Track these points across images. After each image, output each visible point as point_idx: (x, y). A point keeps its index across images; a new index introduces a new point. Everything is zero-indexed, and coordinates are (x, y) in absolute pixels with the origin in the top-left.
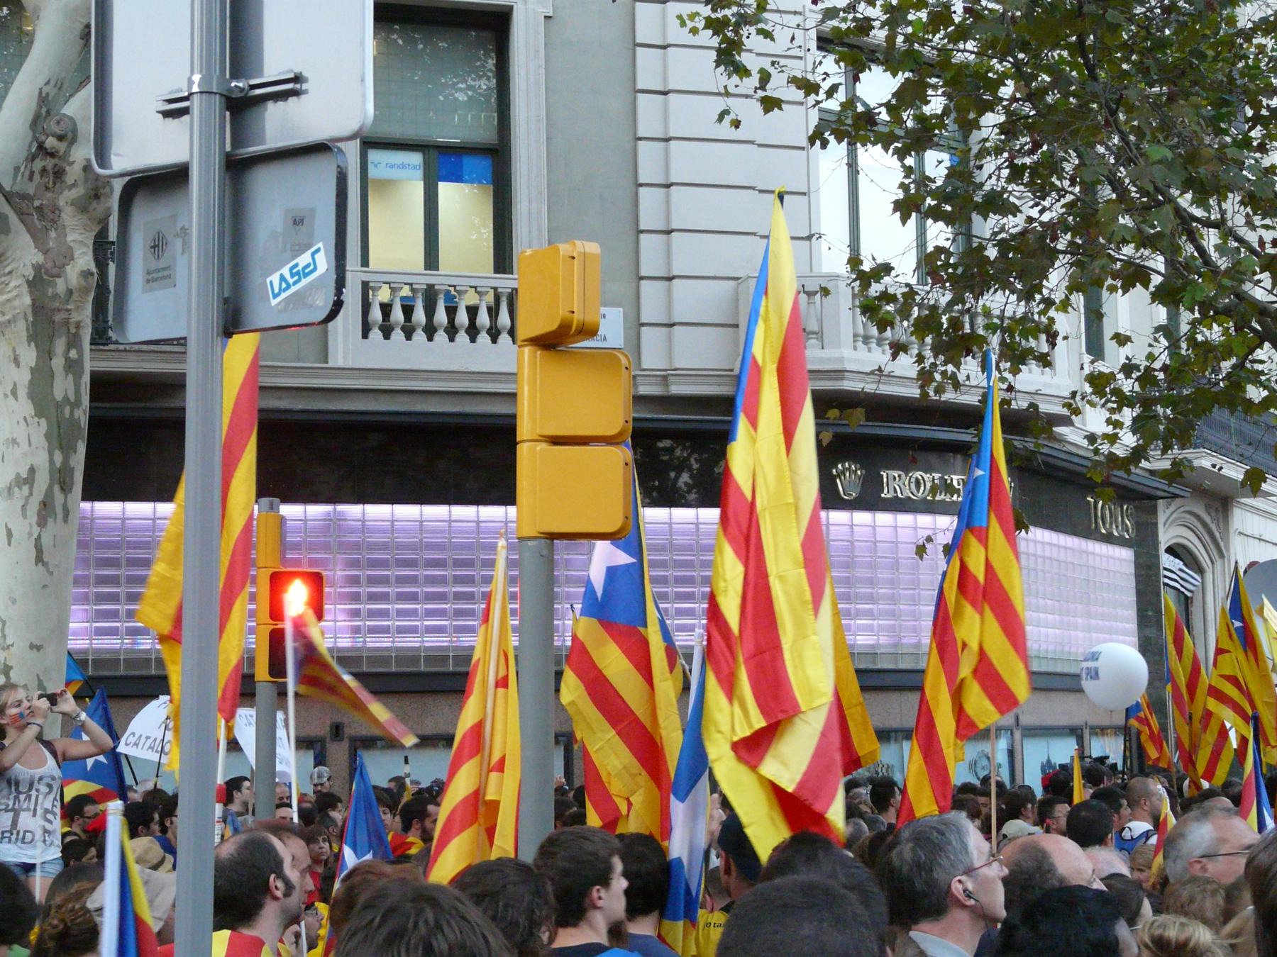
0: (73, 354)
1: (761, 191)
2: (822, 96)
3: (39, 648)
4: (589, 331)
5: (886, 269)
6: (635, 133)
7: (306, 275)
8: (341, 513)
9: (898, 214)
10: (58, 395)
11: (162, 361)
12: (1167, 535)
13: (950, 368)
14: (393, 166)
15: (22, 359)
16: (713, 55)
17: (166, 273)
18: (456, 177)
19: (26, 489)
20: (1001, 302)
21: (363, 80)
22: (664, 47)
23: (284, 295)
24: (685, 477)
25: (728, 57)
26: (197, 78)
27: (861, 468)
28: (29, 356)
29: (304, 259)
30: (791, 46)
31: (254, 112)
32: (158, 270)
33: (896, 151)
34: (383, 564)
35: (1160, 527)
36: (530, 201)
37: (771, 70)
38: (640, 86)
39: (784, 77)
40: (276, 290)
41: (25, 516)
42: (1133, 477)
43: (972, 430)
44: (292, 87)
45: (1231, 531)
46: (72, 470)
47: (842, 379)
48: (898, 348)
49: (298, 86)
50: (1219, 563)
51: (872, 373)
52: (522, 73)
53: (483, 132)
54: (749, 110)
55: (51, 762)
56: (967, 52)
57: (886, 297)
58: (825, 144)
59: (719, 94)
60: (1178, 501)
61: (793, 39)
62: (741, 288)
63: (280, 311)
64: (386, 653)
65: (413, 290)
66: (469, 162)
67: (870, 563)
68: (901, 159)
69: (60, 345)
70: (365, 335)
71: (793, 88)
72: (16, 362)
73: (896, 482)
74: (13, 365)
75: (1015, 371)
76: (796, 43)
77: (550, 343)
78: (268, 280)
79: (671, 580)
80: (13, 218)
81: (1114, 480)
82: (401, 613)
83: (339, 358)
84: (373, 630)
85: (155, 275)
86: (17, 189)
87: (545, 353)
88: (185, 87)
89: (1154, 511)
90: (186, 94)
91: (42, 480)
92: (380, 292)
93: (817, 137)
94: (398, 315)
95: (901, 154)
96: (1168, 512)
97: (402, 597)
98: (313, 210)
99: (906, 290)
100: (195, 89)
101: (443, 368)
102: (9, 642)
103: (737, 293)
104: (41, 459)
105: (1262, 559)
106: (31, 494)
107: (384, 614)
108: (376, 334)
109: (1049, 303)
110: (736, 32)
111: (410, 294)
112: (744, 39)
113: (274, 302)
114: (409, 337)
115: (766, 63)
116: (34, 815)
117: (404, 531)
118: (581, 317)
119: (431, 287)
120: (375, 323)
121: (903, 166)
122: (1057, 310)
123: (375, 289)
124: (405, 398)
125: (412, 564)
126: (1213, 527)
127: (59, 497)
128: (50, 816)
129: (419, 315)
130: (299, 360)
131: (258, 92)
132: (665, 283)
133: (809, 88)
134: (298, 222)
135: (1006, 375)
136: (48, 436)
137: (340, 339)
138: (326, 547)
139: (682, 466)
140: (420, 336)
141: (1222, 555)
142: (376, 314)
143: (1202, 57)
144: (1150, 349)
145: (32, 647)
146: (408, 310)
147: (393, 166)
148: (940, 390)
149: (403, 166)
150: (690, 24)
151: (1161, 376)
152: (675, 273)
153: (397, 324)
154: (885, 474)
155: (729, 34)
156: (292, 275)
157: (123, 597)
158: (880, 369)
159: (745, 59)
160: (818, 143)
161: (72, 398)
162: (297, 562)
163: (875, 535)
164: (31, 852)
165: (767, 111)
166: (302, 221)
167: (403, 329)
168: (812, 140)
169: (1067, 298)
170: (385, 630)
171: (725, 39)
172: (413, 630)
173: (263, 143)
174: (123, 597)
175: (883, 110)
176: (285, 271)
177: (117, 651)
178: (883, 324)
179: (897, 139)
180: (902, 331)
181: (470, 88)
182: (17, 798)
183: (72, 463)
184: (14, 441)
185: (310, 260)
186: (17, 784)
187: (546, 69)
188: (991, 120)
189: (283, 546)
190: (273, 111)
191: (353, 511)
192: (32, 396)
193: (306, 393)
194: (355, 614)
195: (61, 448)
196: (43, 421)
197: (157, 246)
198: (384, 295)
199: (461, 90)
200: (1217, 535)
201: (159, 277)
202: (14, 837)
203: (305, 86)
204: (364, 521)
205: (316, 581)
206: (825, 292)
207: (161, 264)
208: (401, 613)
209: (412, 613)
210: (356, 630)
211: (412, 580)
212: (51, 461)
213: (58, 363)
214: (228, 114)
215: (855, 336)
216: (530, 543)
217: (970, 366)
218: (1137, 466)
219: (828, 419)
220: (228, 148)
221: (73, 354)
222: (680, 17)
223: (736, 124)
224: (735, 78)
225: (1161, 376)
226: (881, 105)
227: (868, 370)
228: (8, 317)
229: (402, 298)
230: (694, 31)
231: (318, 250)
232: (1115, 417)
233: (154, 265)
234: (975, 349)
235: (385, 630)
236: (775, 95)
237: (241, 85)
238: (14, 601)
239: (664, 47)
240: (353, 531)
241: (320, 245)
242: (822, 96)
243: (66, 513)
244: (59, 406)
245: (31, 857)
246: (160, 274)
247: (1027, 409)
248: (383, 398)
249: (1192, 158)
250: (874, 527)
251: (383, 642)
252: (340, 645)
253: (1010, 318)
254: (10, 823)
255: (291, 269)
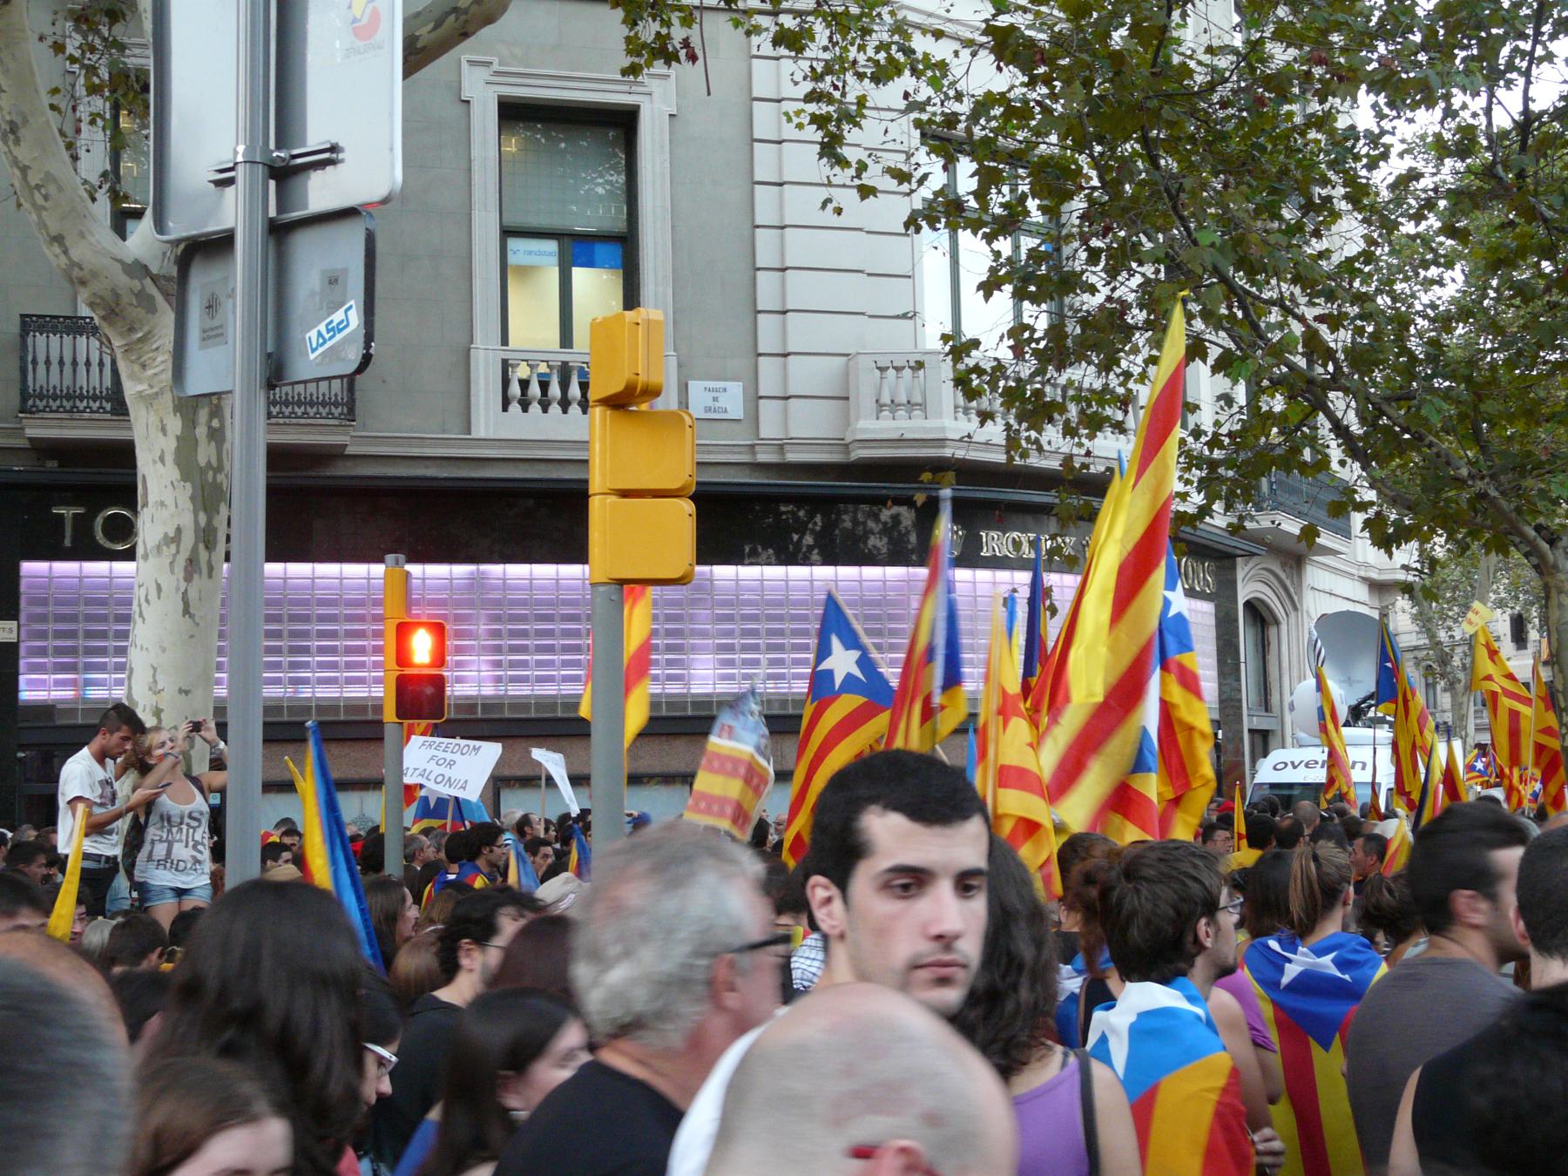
0: (215, 423)
1: (869, 275)
2: (914, 186)
3: (187, 692)
4: (652, 392)
5: (976, 344)
6: (753, 220)
7: (340, 331)
8: (483, 573)
9: (981, 292)
10: (202, 461)
11: (321, 434)
12: (1244, 592)
13: (1033, 434)
14: (530, 253)
15: (168, 428)
16: (817, 148)
17: (219, 331)
18: (590, 263)
19: (173, 547)
20: (1084, 375)
21: (391, 149)
22: (780, 142)
23: (320, 350)
24: (809, 540)
25: (830, 149)
26: (241, 148)
27: (962, 529)
28: (175, 425)
29: (338, 316)
30: (885, 139)
31: (297, 181)
32: (212, 329)
33: (985, 236)
34: (523, 619)
35: (1240, 585)
36: (656, 285)
37: (869, 162)
38: (757, 178)
39: (879, 168)
40: (314, 346)
41: (172, 572)
42: (1198, 533)
43: (1053, 492)
44: (330, 157)
45: (1305, 585)
46: (215, 530)
47: (943, 447)
48: (985, 416)
49: (334, 156)
50: (1293, 615)
51: (961, 440)
52: (649, 166)
53: (620, 225)
54: (848, 198)
55: (199, 797)
56: (1050, 145)
57: (977, 370)
58: (918, 230)
59: (823, 185)
60: (1255, 560)
61: (886, 132)
62: (851, 363)
63: (318, 365)
64: (524, 701)
65: (549, 366)
66: (601, 250)
67: (971, 616)
68: (989, 243)
69: (203, 415)
70: (505, 409)
71: (887, 177)
72: (164, 430)
73: (995, 542)
74: (161, 434)
75: (1091, 437)
76: (890, 136)
77: (619, 403)
78: (307, 336)
79: (788, 632)
80: (159, 298)
81: (1182, 535)
82: (540, 664)
83: (480, 430)
84: (514, 679)
85: (210, 333)
86: (163, 272)
87: (617, 414)
88: (231, 156)
89: (1233, 568)
90: (231, 165)
91: (188, 539)
92: (518, 369)
93: (912, 223)
94: (535, 389)
95: (989, 239)
96: (1247, 569)
97: (541, 649)
98: (346, 270)
99: (995, 363)
100: (240, 159)
101: (577, 439)
102: (160, 687)
103: (847, 364)
104: (187, 520)
105: (1330, 611)
106: (178, 552)
107: (524, 664)
108: (515, 408)
109: (1127, 375)
110: (838, 127)
111: (548, 371)
112: (845, 133)
113: (312, 356)
114: (545, 410)
115: (863, 156)
116: (187, 846)
117: (542, 588)
118: (645, 379)
119: (565, 364)
120: (514, 397)
121: (992, 251)
122: (1136, 381)
123: (515, 366)
124: (542, 466)
125: (548, 618)
126: (1288, 583)
127: (203, 554)
128: (200, 847)
129: (555, 390)
130: (444, 432)
131: (299, 161)
132: (781, 359)
133: (902, 177)
134: (333, 281)
135: (1084, 440)
136: (192, 498)
137: (482, 411)
138: (470, 603)
139: (802, 529)
140: (555, 409)
141: (1295, 608)
142: (515, 389)
143: (1263, 149)
144: (1217, 417)
145: (181, 691)
146: (544, 386)
147: (530, 253)
148: (1024, 455)
149: (541, 254)
150: (796, 120)
151: (1227, 441)
152: (790, 350)
153: (534, 398)
154: (983, 534)
155: (832, 129)
156: (328, 331)
157: (285, 650)
158: (969, 436)
159: (846, 152)
160: (912, 229)
161: (215, 464)
162: (418, 616)
163: (975, 590)
164: (183, 878)
165: (863, 198)
166: (336, 280)
167: (540, 402)
168: (907, 225)
169: (1144, 371)
170: (524, 679)
171: (829, 134)
172: (550, 679)
173: (307, 208)
174: (285, 650)
175: (971, 197)
176: (322, 327)
177: (281, 699)
178: (972, 394)
179: (985, 224)
180: (987, 401)
181: (607, 182)
182: (169, 831)
183: (216, 523)
184: (162, 504)
185: (343, 317)
186: (169, 821)
187: (671, 165)
188: (1078, 204)
189: (409, 603)
190: (316, 180)
191: (495, 570)
192: (178, 462)
193: (501, 463)
194: (498, 664)
195: (205, 510)
196: (188, 485)
197: (211, 307)
198: (522, 371)
199: (599, 184)
200: (1292, 590)
201: (213, 335)
202: (168, 865)
203: (341, 156)
204: (504, 580)
205: (438, 630)
206: (920, 365)
207: (216, 323)
208: (540, 664)
209: (550, 664)
210: (498, 680)
211: (549, 633)
212: (196, 522)
213: (201, 431)
214: (272, 184)
215: (956, 407)
216: (601, 589)
217: (1052, 435)
218: (1201, 522)
219: (922, 482)
220: (272, 213)
221: (215, 423)
222: (786, 114)
223: (839, 211)
224: (837, 169)
225: (1227, 441)
226: (969, 194)
227: (958, 437)
228: (155, 390)
229: (540, 375)
230: (800, 126)
231: (351, 307)
232: (1186, 476)
233: (209, 324)
234: (1056, 416)
235: (524, 679)
236: (870, 183)
237: (282, 155)
238: (164, 650)
239: (780, 142)
240: (494, 588)
241: (352, 302)
242: (914, 186)
243: (211, 569)
244: (203, 471)
245: (183, 883)
246: (214, 333)
247: (1104, 473)
248: (523, 466)
249: (1239, 242)
250: (974, 583)
251: (523, 690)
252: (483, 693)
253: (1088, 390)
254: (164, 852)
255: (327, 325)
